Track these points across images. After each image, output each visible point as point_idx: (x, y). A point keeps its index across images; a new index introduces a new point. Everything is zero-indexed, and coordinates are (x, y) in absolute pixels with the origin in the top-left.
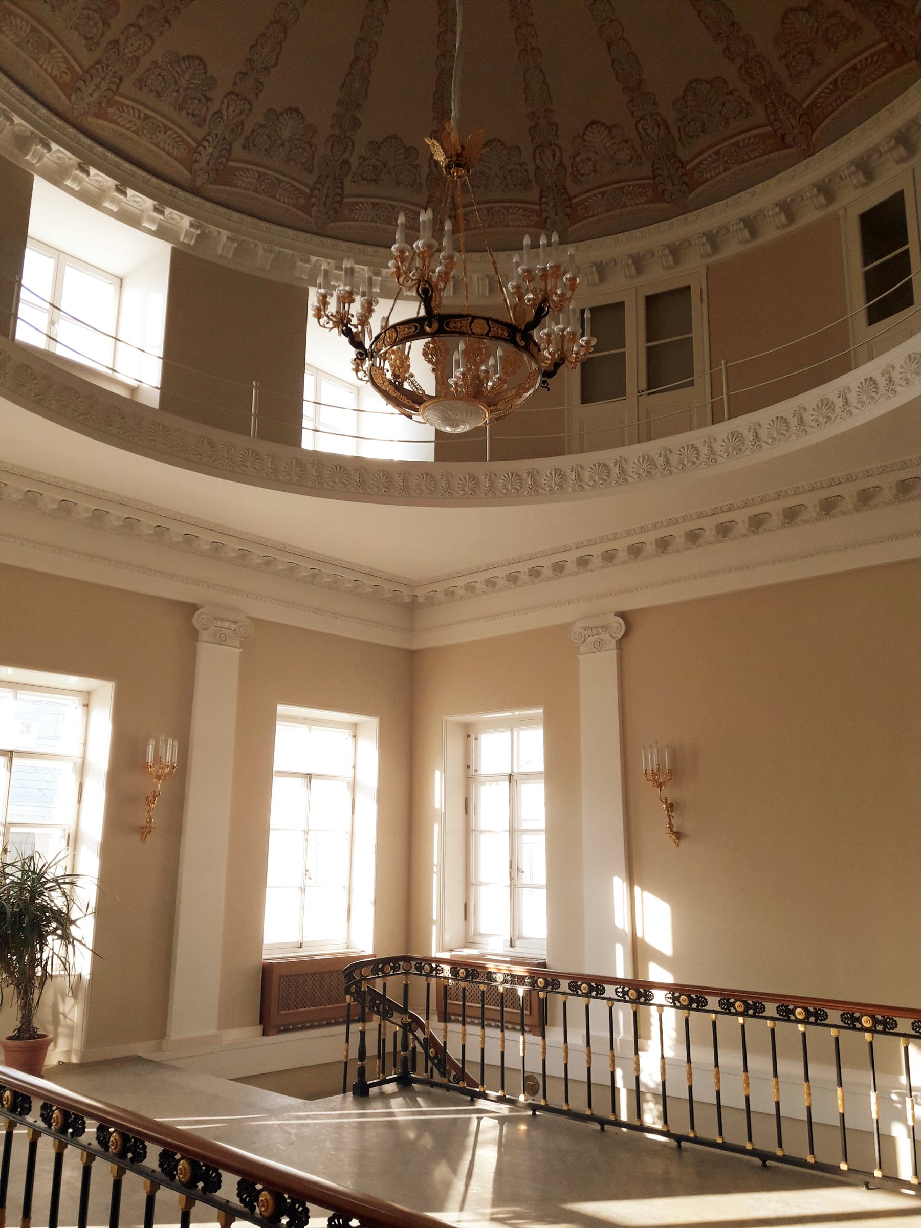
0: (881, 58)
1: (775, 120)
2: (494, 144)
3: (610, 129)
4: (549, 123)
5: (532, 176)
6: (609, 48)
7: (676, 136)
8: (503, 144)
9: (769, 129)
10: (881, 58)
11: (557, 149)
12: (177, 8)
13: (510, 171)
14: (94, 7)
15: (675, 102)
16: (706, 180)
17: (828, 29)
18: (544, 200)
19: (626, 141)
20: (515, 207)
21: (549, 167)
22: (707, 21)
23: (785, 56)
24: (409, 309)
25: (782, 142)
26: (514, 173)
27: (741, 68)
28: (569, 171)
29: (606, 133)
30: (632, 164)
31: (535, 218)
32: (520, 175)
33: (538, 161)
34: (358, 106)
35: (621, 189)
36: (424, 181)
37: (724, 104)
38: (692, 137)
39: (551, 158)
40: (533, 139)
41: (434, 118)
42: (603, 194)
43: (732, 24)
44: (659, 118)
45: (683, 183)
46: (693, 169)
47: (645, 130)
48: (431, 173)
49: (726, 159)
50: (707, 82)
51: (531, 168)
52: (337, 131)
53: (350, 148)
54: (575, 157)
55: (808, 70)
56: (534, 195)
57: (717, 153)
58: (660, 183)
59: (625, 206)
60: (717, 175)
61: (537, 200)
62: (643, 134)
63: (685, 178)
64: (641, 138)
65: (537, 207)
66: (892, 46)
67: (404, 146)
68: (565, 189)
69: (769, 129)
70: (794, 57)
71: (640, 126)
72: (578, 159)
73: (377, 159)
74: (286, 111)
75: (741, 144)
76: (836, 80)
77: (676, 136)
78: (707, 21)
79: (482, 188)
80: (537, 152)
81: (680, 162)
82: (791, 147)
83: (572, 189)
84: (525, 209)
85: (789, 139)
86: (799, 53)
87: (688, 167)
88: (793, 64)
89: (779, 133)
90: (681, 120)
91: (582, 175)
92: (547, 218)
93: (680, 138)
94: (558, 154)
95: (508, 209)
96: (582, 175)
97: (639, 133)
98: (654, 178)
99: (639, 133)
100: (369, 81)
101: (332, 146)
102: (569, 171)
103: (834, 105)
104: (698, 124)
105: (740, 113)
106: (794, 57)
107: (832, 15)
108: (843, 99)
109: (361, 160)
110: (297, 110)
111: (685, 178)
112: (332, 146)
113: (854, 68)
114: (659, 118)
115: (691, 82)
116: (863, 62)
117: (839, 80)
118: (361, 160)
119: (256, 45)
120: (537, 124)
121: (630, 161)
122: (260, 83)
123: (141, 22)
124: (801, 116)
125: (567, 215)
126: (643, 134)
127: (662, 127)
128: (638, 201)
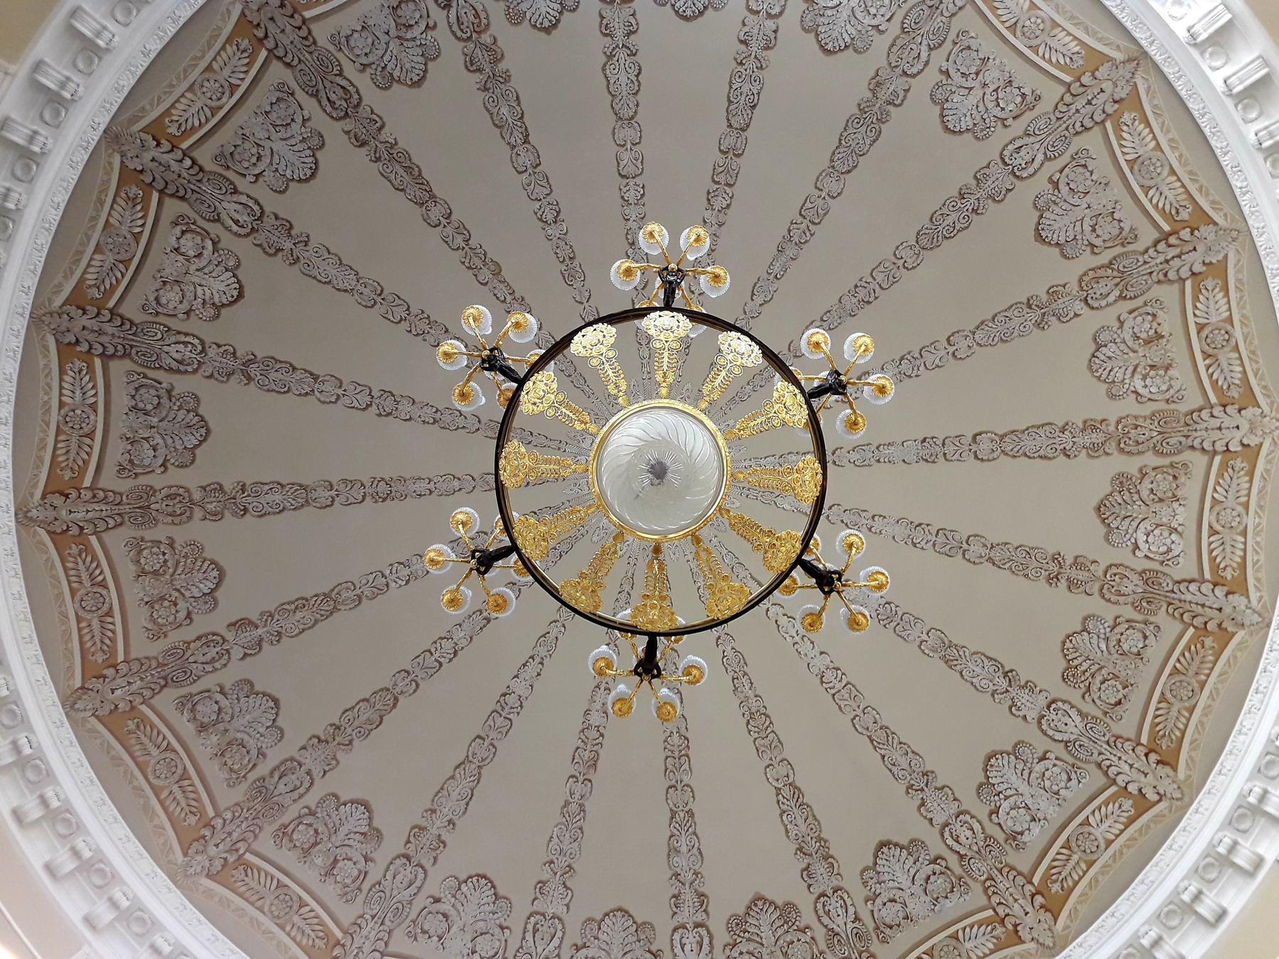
0: (105, 648)
1: (94, 496)
2: (309, 173)
3: (219, 307)
4: (279, 250)
5: (230, 174)
6: (311, 374)
7: (150, 373)
8: (300, 181)
9: (87, 483)
10: (105, 648)
11: (242, 231)
12: (741, 64)
13: (259, 159)
14: (829, 12)
15: (197, 398)
16: (62, 372)
17: (176, 605)
18: (188, 162)
19: (187, 313)
20: (207, 120)
21: (225, 204)
22: (267, 487)
23: (171, 544)
24: (1026, 838)
25: (57, 489)
26: (254, 160)
27: (187, 490)
28: (201, 222)
29: (216, 300)
30: (152, 299)
31: (173, 130)
32: (246, 164)
33: (244, 199)
34: (486, 89)
35: (126, 263)
36: (340, 56)
37: (155, 450)
38: (137, 389)
39: (237, 216)
40: (277, 218)
41: (396, 144)
42: (137, 237)
43: (245, 510)
44: (189, 369)
45: (78, 342)
46: (90, 369)
47: (186, 344)
48: (340, 74)
49: (78, 412)
50: (196, 447)
51: (242, 184)
52: (486, 38)
53: (455, 28)
54: (214, 243)
55: (138, 561)
56: (205, 156)
57: (93, 407)
58: (98, 314)
59: (98, 249)
60: (61, 388)
61: (195, 154)
62: (183, 338)
63: (84, 347)
64: (179, 333)
65: (184, 146)
66: (114, 666)
67: (399, 81)
68: (182, 198)
69: (87, 483)
70: (164, 554)
71: (196, 342)
72: (209, 244)
73: (414, 39)
74: (558, 21)
75: (88, 441)
76: (106, 587)
77: (150, 373)
78: (267, 487)
79: (268, 109)
80: (256, 208)
81: (113, 356)
82: (44, 497)
83: (174, 208)
84: (193, 130)
85: (58, 500)
86: (166, 561)
87: (98, 362)
88: (155, 550)
89: (74, 494)
90: (169, 392)
91: (183, 232)
92: (158, 144)
93: (145, 377)
94: (235, 228)
95: (214, 111)
96: (183, 232)
97: (186, 334)
98: (111, 311)
99: (186, 334)
100: (496, 125)
101: (477, 15)
102: (201, 222)
103: (72, 572)
104: (149, 407)
105: (131, 461)
106: (164, 554)
107: (189, 616)
108: (74, 585)
109: (431, 24)
110: (547, 31)
111: (84, 347)
112: (477, 15)
113: (109, 613)
114: (189, 369)
115: (208, 432)
116: (111, 627)
117: (104, 592)
118: (431, 24)
119: (637, 76)
120: (290, 236)
121: (157, 299)
122: (606, 35)
123: (770, 24)
124: (81, 528)
125: (141, 171)
126: (183, 338)
127: (174, 365)
128: (91, 270)
